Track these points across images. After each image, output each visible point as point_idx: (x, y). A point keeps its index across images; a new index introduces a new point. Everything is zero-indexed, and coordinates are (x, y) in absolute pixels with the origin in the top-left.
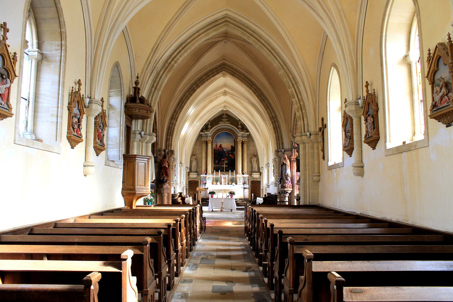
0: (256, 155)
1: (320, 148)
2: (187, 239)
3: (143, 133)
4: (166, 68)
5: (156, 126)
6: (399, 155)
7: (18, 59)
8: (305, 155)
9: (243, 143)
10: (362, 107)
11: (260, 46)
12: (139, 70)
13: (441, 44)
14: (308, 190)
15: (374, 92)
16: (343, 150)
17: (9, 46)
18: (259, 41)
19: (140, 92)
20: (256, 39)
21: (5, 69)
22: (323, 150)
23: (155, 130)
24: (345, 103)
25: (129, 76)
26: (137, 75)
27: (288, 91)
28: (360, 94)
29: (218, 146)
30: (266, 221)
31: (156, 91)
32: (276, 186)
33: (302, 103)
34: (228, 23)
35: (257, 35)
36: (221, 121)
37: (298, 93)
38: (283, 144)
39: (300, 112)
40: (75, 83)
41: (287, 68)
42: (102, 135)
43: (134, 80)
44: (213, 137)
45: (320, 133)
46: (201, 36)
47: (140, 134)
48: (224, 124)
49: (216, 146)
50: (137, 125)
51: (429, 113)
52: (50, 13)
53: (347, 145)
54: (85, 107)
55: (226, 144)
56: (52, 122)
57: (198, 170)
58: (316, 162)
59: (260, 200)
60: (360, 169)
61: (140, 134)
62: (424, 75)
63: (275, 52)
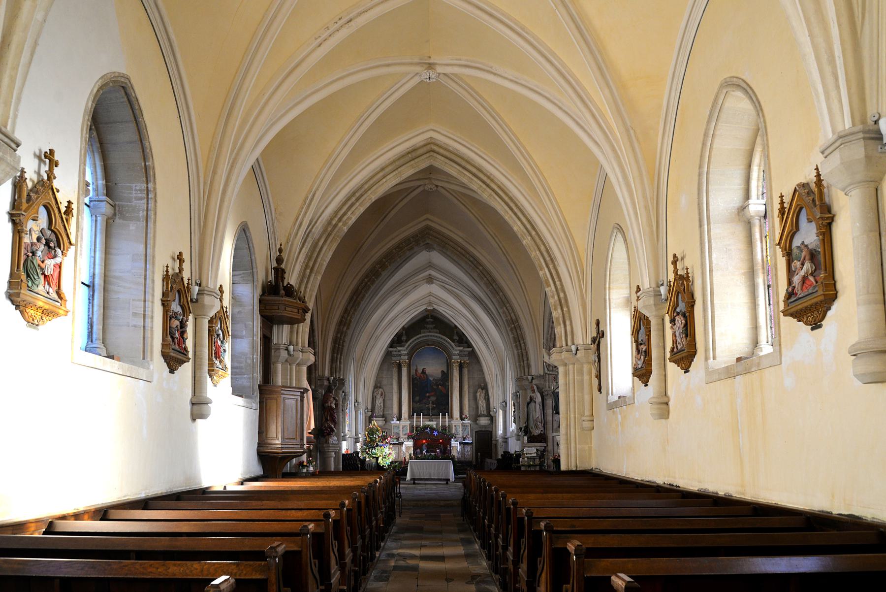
0: (485, 388)
1: (594, 372)
2: (354, 551)
3: (291, 348)
4: (329, 235)
5: (314, 336)
6: (730, 380)
7: (75, 212)
8: (567, 384)
9: (461, 367)
10: (666, 300)
11: (491, 195)
12: (281, 239)
13: (804, 185)
14: (573, 445)
15: (688, 273)
16: (634, 375)
17: (58, 191)
18: (488, 186)
19: (286, 276)
20: (484, 182)
21: (52, 231)
22: (599, 377)
23: (312, 343)
24: (637, 292)
25: (265, 250)
26: (278, 246)
27: (538, 274)
28: (662, 277)
29: (420, 371)
30: (504, 496)
31: (313, 275)
32: (519, 439)
33: (562, 295)
34: (435, 155)
35: (485, 175)
36: (425, 328)
37: (555, 277)
38: (529, 366)
39: (559, 311)
40: (173, 259)
41: (537, 234)
42: (222, 350)
43: (275, 254)
44: (410, 355)
45: (594, 347)
46: (388, 177)
47: (287, 349)
48: (430, 328)
49: (416, 371)
50: (282, 335)
51: (782, 306)
52: (127, 134)
53: (640, 366)
54: (191, 300)
55: (433, 368)
56: (135, 326)
57: (386, 413)
58: (587, 398)
59: (491, 463)
60: (663, 406)
61: (287, 349)
62: (774, 240)
63: (516, 205)
